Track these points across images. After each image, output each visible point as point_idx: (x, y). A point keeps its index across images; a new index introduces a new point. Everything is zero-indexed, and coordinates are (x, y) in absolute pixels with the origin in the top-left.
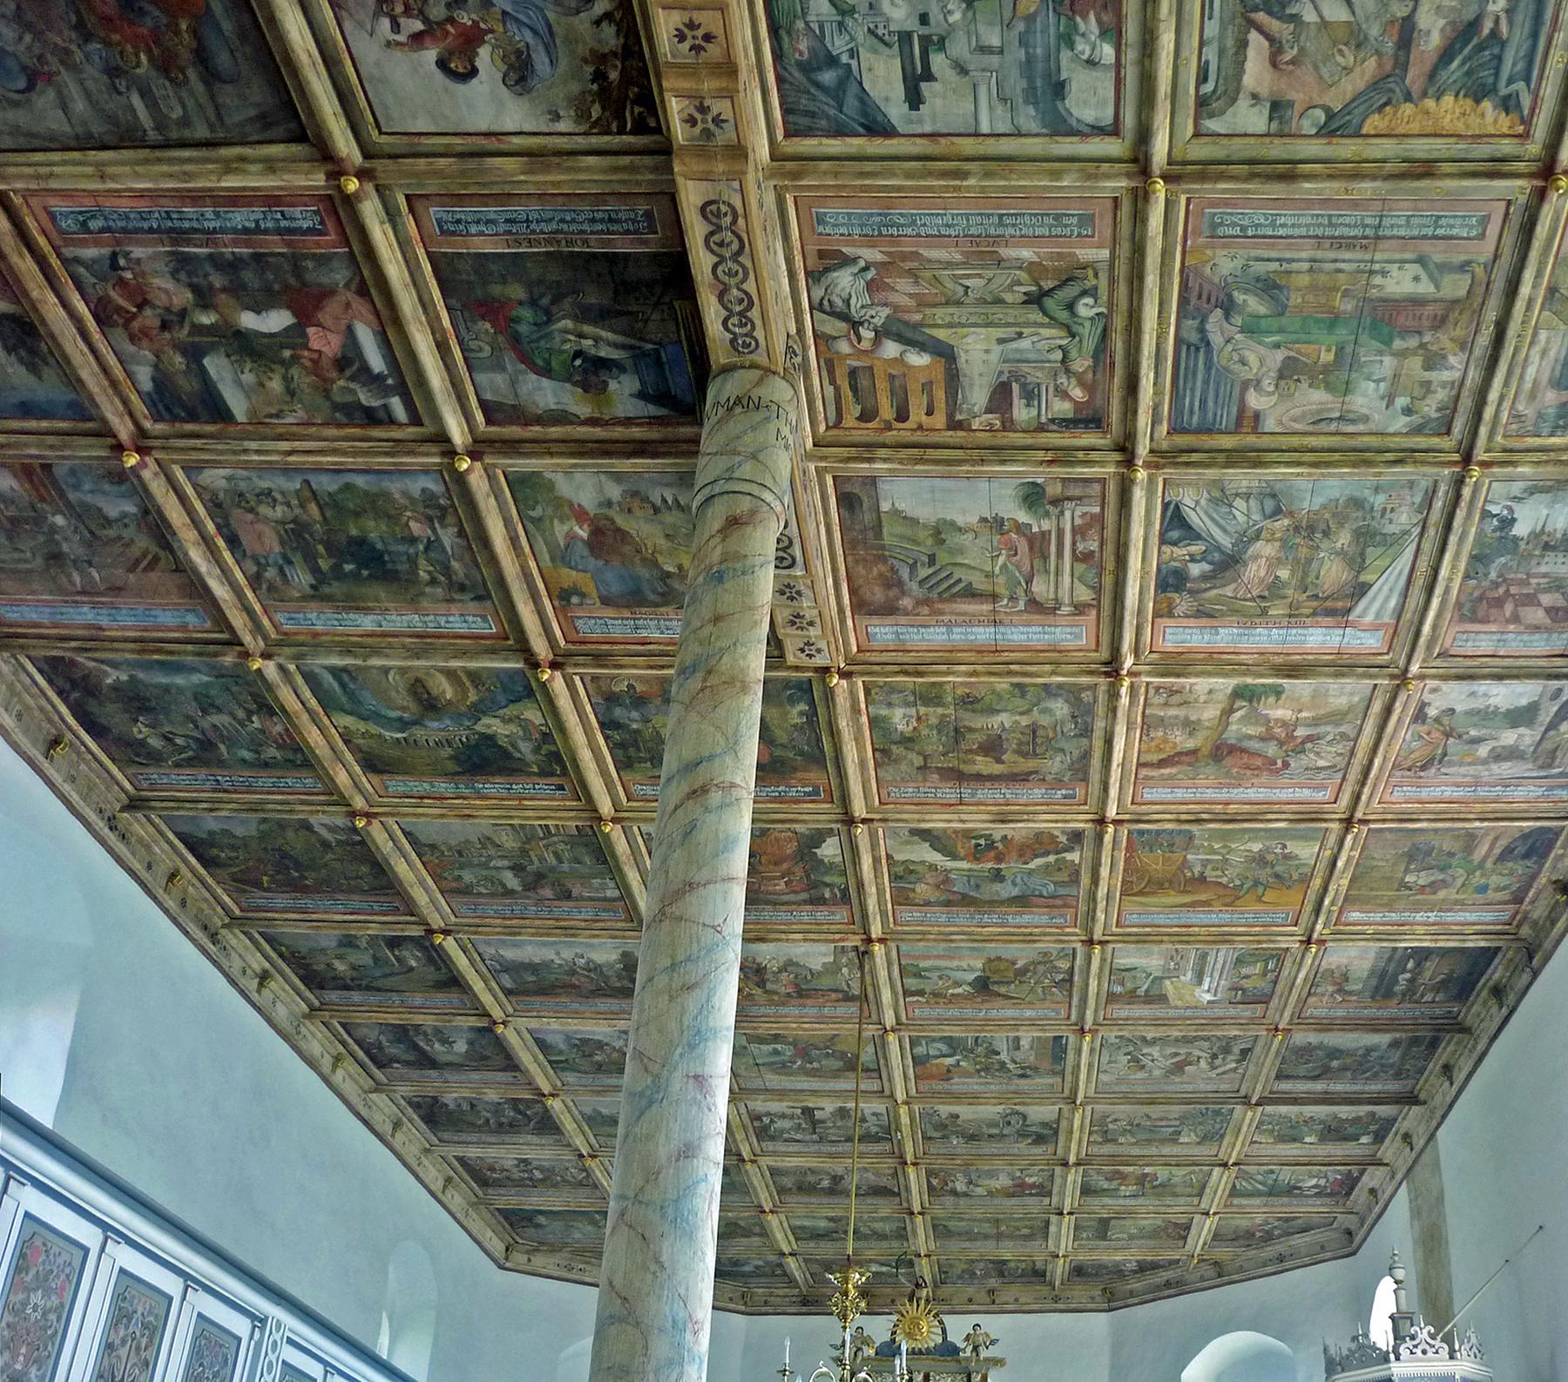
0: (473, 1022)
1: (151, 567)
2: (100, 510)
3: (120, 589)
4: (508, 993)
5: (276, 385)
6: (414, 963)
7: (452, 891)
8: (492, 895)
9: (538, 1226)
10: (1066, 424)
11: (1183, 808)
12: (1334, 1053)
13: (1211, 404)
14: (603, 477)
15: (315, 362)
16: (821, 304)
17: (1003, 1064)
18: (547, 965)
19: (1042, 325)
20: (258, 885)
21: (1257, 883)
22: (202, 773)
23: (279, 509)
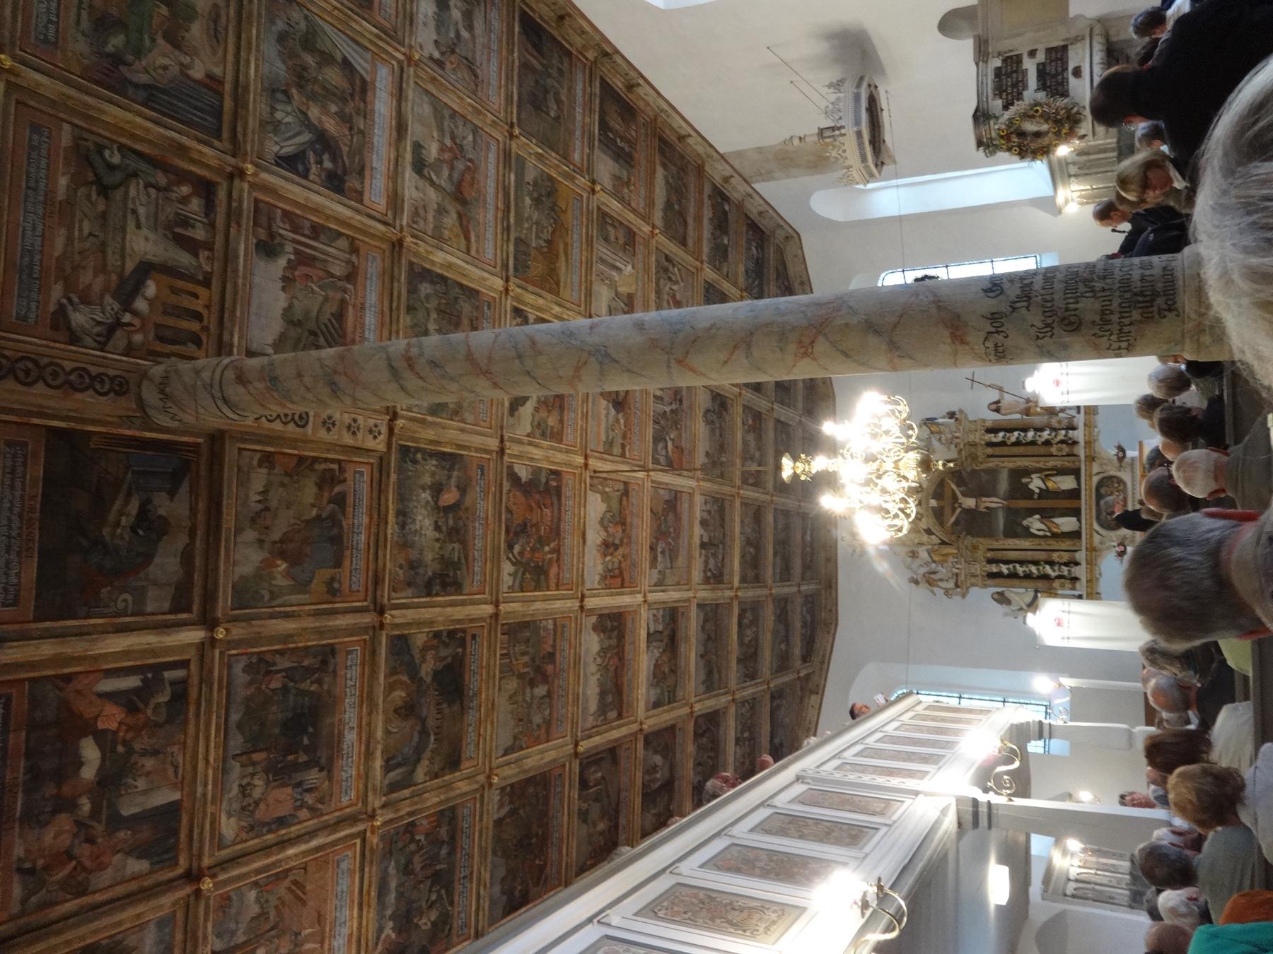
0: (640, 745)
1: (301, 886)
2: (253, 918)
3: (319, 914)
4: (620, 716)
5: (149, 763)
6: (599, 775)
7: (548, 732)
8: (551, 706)
9: (781, 744)
10: (209, 207)
11: (499, 237)
12: (668, 206)
13: (199, 104)
14: (239, 540)
15: (130, 728)
16: (99, 342)
17: (672, 411)
18: (601, 685)
19: (127, 193)
20: (542, 868)
21: (552, 209)
22: (458, 888)
23: (256, 782)
